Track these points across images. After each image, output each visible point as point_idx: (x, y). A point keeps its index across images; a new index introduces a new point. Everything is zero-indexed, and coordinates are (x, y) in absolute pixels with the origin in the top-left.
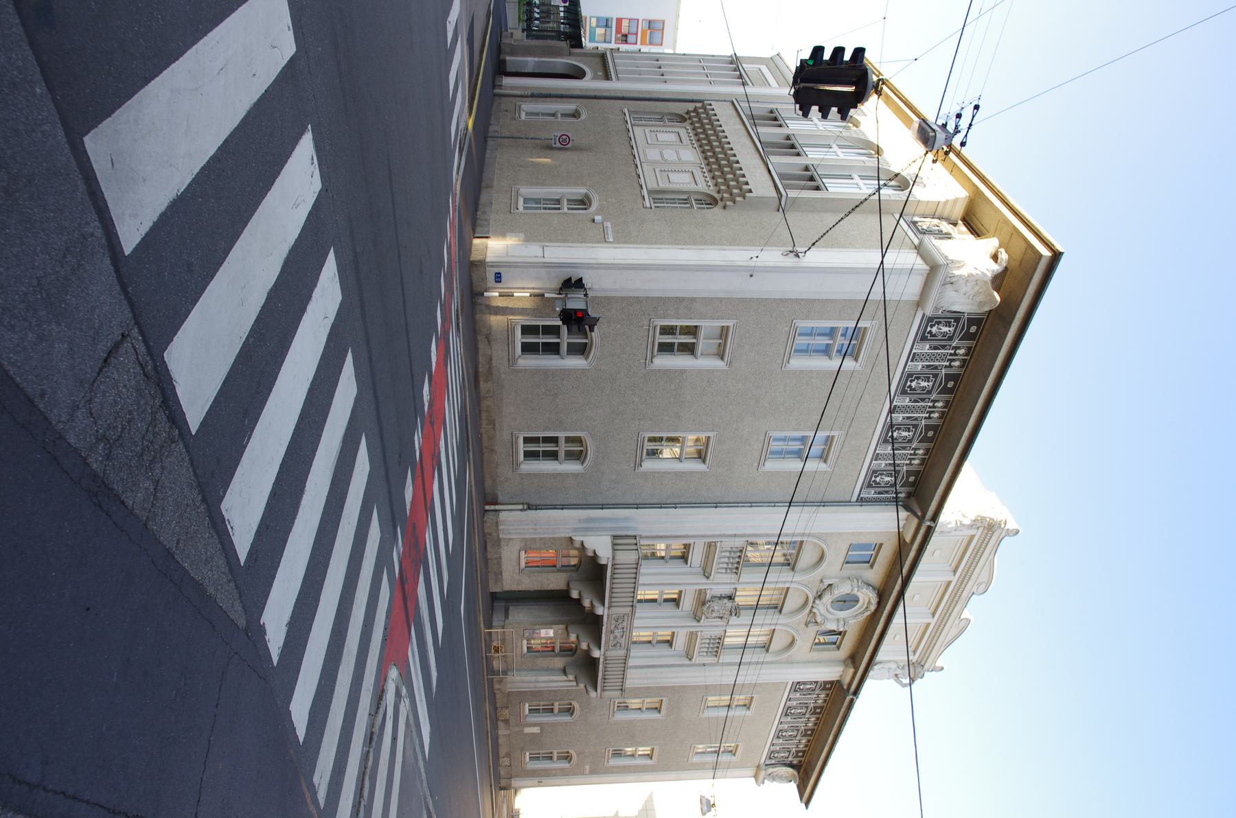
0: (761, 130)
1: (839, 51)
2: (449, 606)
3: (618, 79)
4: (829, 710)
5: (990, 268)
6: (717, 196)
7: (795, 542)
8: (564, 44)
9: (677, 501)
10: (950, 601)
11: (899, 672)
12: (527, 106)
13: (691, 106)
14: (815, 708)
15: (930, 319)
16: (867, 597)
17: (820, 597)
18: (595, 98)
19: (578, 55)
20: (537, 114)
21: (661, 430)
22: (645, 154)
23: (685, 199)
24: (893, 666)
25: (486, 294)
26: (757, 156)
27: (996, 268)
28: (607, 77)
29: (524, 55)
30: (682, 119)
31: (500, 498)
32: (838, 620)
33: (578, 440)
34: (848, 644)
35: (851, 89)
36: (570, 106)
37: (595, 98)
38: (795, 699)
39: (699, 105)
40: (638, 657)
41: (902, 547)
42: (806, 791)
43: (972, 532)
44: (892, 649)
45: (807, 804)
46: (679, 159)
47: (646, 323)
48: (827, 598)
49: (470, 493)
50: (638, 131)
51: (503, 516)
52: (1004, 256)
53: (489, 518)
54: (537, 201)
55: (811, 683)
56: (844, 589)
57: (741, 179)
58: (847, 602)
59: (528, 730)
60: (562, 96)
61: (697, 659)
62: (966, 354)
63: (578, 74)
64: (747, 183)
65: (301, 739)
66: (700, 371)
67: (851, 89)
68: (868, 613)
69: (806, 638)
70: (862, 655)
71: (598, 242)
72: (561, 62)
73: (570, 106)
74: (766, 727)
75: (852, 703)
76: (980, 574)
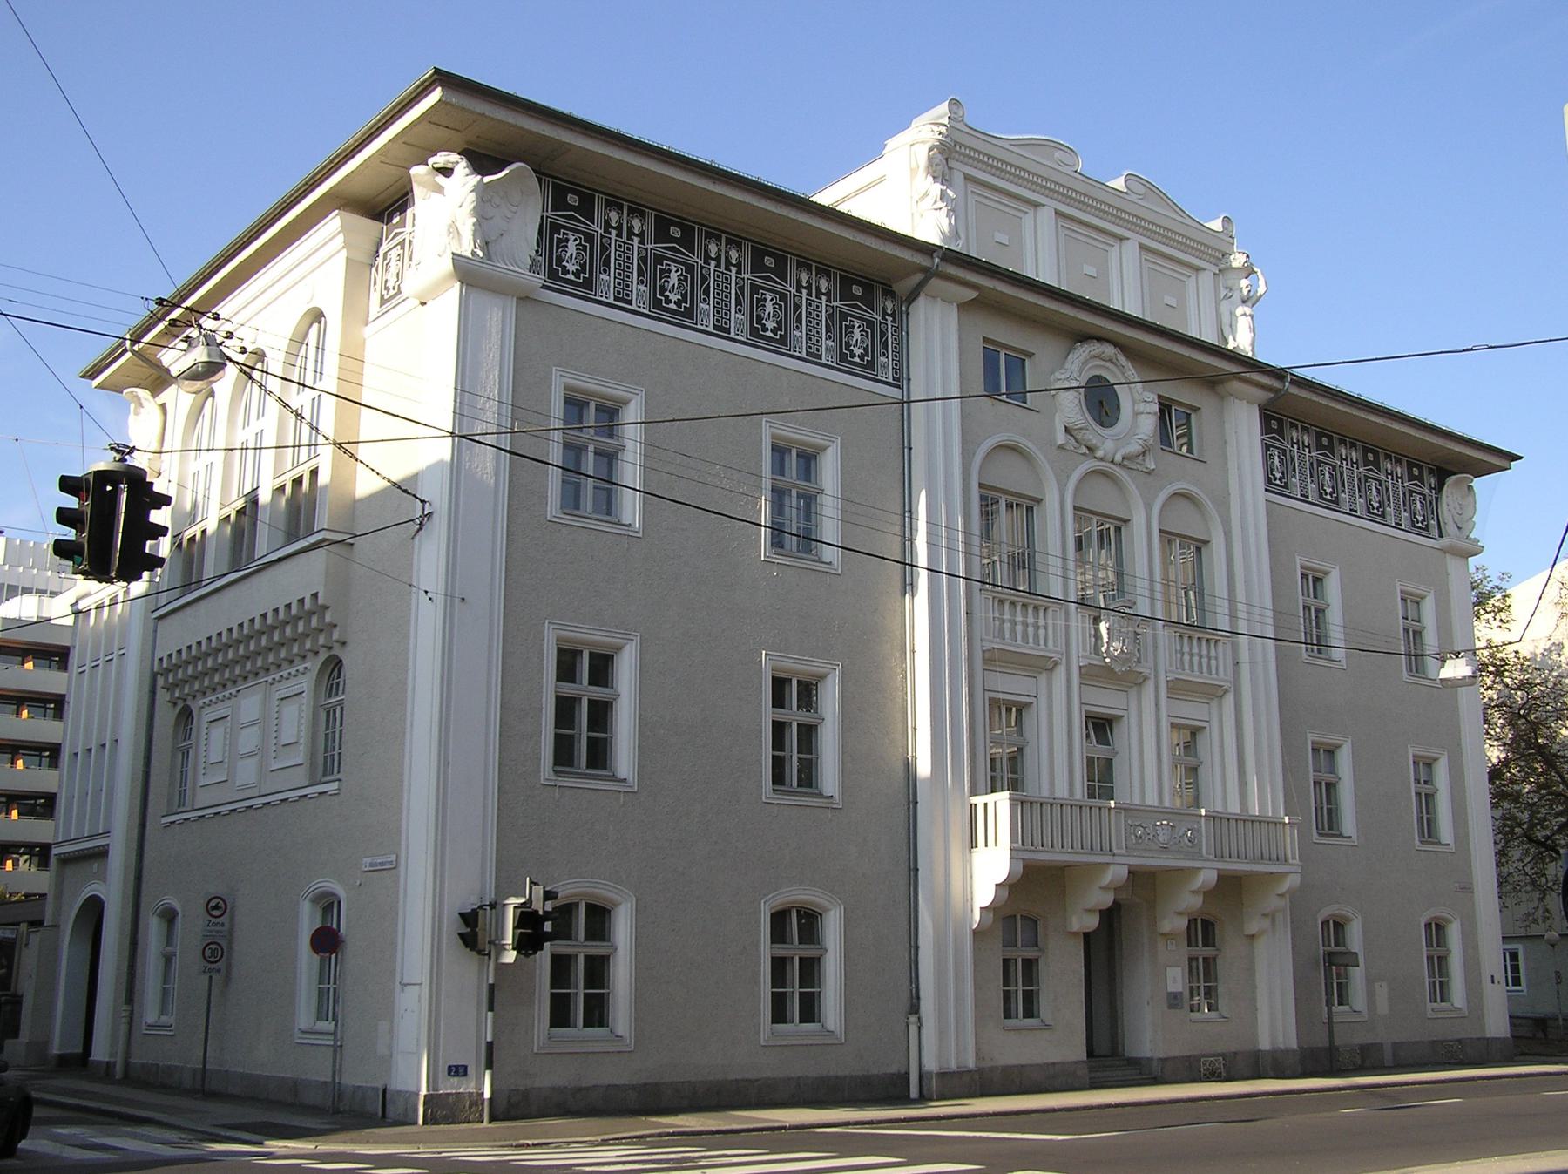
0: (209, 573)
1: (64, 516)
3: (107, 833)
5: (464, 181)
6: (324, 655)
7: (983, 498)
10: (1091, 214)
12: (150, 1014)
13: (163, 696)
14: (1320, 447)
15: (553, 275)
16: (1080, 364)
19: (58, 910)
20: (165, 992)
22: (247, 787)
23: (330, 721)
26: (254, 579)
27: (462, 167)
28: (102, 854)
30: (186, 716)
32: (1136, 414)
33: (779, 919)
34: (1183, 393)
37: (147, 775)
38: (1304, 487)
39: (160, 681)
40: (1222, 794)
41: (983, 304)
43: (958, 178)
44: (1125, 287)
46: (255, 723)
50: (203, 798)
51: (931, 1065)
52: (441, 159)
54: (322, 994)
55: (1267, 459)
56: (1070, 408)
57: (294, 610)
58: (1101, 401)
59: (1383, 1007)
61: (1223, 676)
62: (620, 208)
63: (94, 908)
64: (301, 601)
68: (1122, 359)
69: (1179, 475)
70: (1195, 370)
71: (397, 882)
73: (153, 928)
74: (1357, 546)
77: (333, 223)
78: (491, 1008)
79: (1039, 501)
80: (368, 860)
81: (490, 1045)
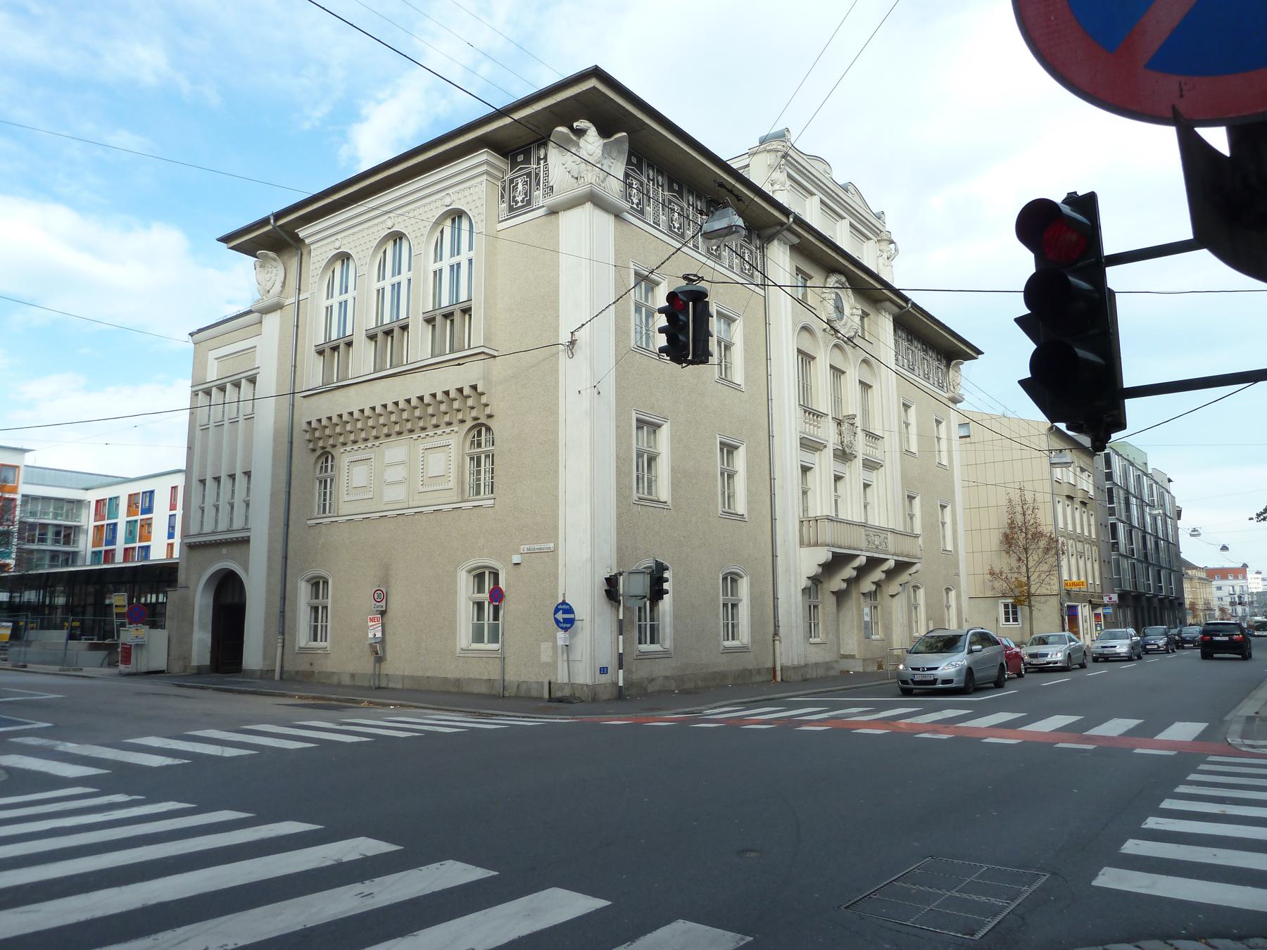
6: (469, 424)
10: (838, 201)
11: (885, 256)
17: (837, 331)
18: (286, 558)
24: (881, 261)
25: (621, 684)
28: (246, 541)
31: (770, 665)
33: (725, 579)
45: (979, 352)
48: (837, 325)
65: (608, 903)
66: (673, 451)
70: (872, 290)
71: (556, 560)
76: (816, 169)
77: (483, 156)
78: (621, 634)
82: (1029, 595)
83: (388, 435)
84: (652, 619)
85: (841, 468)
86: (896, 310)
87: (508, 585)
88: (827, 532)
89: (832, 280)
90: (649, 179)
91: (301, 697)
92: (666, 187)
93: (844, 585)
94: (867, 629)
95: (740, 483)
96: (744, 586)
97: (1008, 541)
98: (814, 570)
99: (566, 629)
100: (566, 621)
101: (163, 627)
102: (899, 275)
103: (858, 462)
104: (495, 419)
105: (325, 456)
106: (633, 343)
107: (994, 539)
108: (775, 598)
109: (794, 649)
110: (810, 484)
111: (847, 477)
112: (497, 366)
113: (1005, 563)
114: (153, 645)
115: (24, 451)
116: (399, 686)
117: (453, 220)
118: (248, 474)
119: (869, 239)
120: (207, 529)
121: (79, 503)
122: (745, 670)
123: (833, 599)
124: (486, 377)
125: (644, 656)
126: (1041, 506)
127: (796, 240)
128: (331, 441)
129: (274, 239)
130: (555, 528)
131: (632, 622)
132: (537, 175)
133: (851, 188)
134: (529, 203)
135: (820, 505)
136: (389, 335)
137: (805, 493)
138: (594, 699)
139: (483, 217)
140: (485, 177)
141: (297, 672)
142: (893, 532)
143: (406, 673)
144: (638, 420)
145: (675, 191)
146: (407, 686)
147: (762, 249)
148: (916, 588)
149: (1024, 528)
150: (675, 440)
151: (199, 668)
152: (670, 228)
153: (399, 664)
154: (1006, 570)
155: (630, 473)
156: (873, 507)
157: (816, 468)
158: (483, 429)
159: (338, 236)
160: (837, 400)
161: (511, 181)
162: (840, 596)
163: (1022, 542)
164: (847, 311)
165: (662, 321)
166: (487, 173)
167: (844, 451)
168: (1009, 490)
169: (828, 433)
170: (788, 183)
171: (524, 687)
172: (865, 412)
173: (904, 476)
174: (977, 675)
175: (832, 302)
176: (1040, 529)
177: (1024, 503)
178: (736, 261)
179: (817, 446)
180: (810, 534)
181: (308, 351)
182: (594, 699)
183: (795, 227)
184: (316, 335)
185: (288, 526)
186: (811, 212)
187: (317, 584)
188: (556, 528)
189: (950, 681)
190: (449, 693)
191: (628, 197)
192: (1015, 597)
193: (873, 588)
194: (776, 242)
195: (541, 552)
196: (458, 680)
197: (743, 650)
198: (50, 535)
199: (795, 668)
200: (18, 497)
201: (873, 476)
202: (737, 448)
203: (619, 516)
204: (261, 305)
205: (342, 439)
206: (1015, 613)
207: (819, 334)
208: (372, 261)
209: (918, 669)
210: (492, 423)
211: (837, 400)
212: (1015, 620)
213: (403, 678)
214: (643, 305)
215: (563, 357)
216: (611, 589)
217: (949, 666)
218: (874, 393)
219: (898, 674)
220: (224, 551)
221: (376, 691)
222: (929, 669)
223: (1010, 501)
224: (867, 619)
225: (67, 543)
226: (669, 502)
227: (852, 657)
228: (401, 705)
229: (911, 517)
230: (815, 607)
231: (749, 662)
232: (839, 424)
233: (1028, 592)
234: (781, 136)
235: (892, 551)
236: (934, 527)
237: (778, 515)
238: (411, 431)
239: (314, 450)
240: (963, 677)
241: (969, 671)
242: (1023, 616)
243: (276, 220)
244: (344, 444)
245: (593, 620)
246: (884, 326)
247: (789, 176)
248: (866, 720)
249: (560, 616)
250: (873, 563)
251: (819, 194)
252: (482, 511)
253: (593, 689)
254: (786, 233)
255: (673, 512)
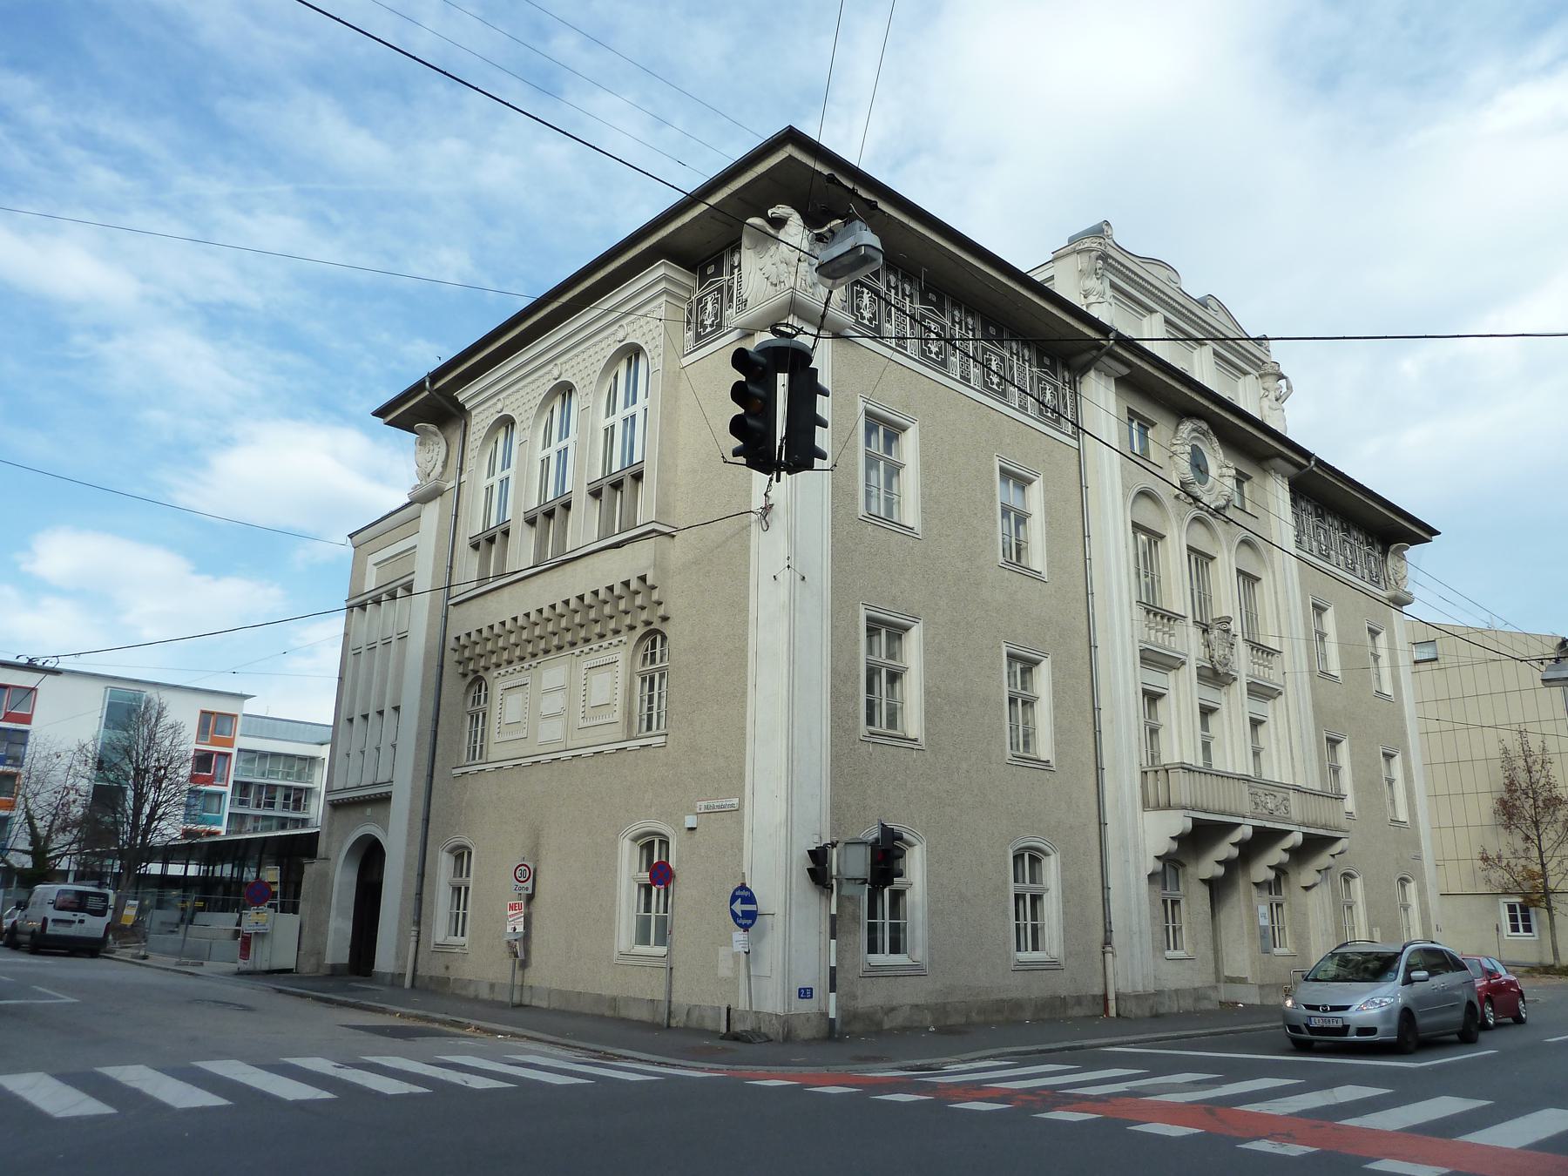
2: (1025, 1059)
4: (1330, 499)
6: (640, 631)
8: (311, 870)
9: (1089, 707)
10: (1197, 322)
11: (1272, 395)
17: (1196, 499)
18: (427, 820)
21: (1001, 728)
25: (832, 1015)
28: (385, 799)
29: (325, 934)
33: (1018, 858)
35: (782, 379)
36: (443, 865)
42: (1421, 532)
47: (864, 748)
48: (1197, 490)
49: (1136, 1043)
53: (1132, 1008)
58: (1199, 465)
60: (422, 875)
66: (928, 665)
67: (782, 379)
70: (1255, 445)
71: (740, 822)
72: (341, 879)
73: (443, 865)
75: (1320, 463)
76: (1156, 276)
77: (660, 269)
78: (833, 936)
79: (1162, 537)
80: (704, 803)
81: (833, 970)
82: (1547, 893)
83: (547, 652)
84: (1034, 917)
85: (1211, 695)
86: (1293, 470)
87: (679, 860)
88: (1182, 787)
89: (1187, 427)
90: (954, 322)
91: (402, 1016)
92: (917, 299)
93: (1220, 871)
94: (1268, 939)
95: (1043, 715)
96: (1051, 869)
97: (1507, 811)
98: (1165, 845)
99: (746, 928)
100: (747, 914)
101: (295, 911)
102: (1299, 421)
103: (1240, 688)
104: (670, 622)
105: (477, 682)
106: (861, 510)
107: (1483, 808)
108: (1105, 888)
109: (1138, 966)
110: (1263, 743)
111: (1223, 709)
112: (677, 551)
113: (1505, 843)
114: (280, 938)
115: (246, 697)
116: (544, 1004)
117: (630, 360)
118: (397, 709)
119: (1246, 373)
120: (367, 780)
121: (312, 760)
122: (1054, 998)
123: (1204, 892)
124: (659, 565)
125: (875, 973)
126: (1556, 759)
127: (1125, 371)
128: (482, 663)
129: (429, 408)
130: (741, 776)
131: (856, 919)
132: (730, 288)
133: (1212, 303)
134: (720, 326)
135: (1179, 745)
136: (550, 515)
137: (1154, 731)
138: (788, 1038)
139: (661, 350)
140: (664, 298)
141: (431, 978)
142: (1298, 790)
143: (554, 986)
144: (869, 619)
145: (930, 302)
146: (554, 1005)
147: (1073, 385)
148: (1348, 877)
149: (1532, 791)
150: (931, 650)
151: (334, 967)
152: (986, 384)
153: (551, 974)
154: (1506, 853)
155: (856, 696)
156: (1272, 755)
157: (1171, 694)
158: (659, 638)
159: (501, 397)
160: (1202, 598)
161: (699, 301)
162: (1217, 889)
163: (1528, 810)
164: (1213, 470)
165: (822, 438)
166: (665, 291)
167: (1215, 671)
168: (1504, 734)
169: (1188, 643)
170: (1109, 292)
171: (695, 1015)
172: (1250, 617)
173: (1317, 708)
174: (1422, 1021)
175: (1186, 457)
176: (1556, 792)
177: (1527, 754)
178: (975, 371)
179: (1171, 662)
180: (1157, 789)
181: (463, 544)
182: (788, 1038)
183: (1120, 351)
184: (474, 525)
185: (431, 776)
186: (1149, 330)
187: (461, 855)
188: (742, 776)
189: (1373, 1031)
190: (601, 1017)
191: (855, 309)
192: (1524, 895)
193: (1271, 875)
194: (1092, 373)
195: (722, 811)
196: (614, 999)
197: (1053, 966)
198: (279, 799)
199: (1138, 997)
200: (234, 751)
201: (1265, 709)
202: (1037, 663)
203: (835, 758)
204: (420, 491)
205: (494, 659)
206: (1526, 919)
207: (1169, 502)
208: (535, 425)
209: (1316, 1008)
210: (668, 629)
211: (1202, 598)
212: (1528, 929)
213: (550, 992)
214: (880, 458)
215: (755, 529)
216: (819, 867)
217: (1371, 1005)
218: (1264, 591)
219: (1285, 1015)
220: (369, 811)
221: (518, 1013)
222: (1334, 1009)
223: (1506, 751)
224: (1265, 922)
225: (297, 808)
226: (922, 740)
227: (1242, 981)
228: (513, 1035)
229: (1336, 771)
230: (1175, 903)
231: (1062, 985)
232: (1205, 631)
233: (1545, 887)
234: (1099, 231)
235: (1298, 821)
236: (1375, 787)
237: (1106, 762)
238: (573, 644)
239: (465, 675)
240: (1394, 1024)
241: (1407, 1014)
242: (1539, 923)
243: (433, 383)
244: (498, 666)
245: (788, 913)
246: (1276, 494)
247: (1113, 286)
248: (1172, 1102)
249: (739, 907)
250: (1265, 838)
251: (1162, 312)
252: (651, 751)
253: (787, 1021)
254: (1105, 359)
255: (928, 753)
